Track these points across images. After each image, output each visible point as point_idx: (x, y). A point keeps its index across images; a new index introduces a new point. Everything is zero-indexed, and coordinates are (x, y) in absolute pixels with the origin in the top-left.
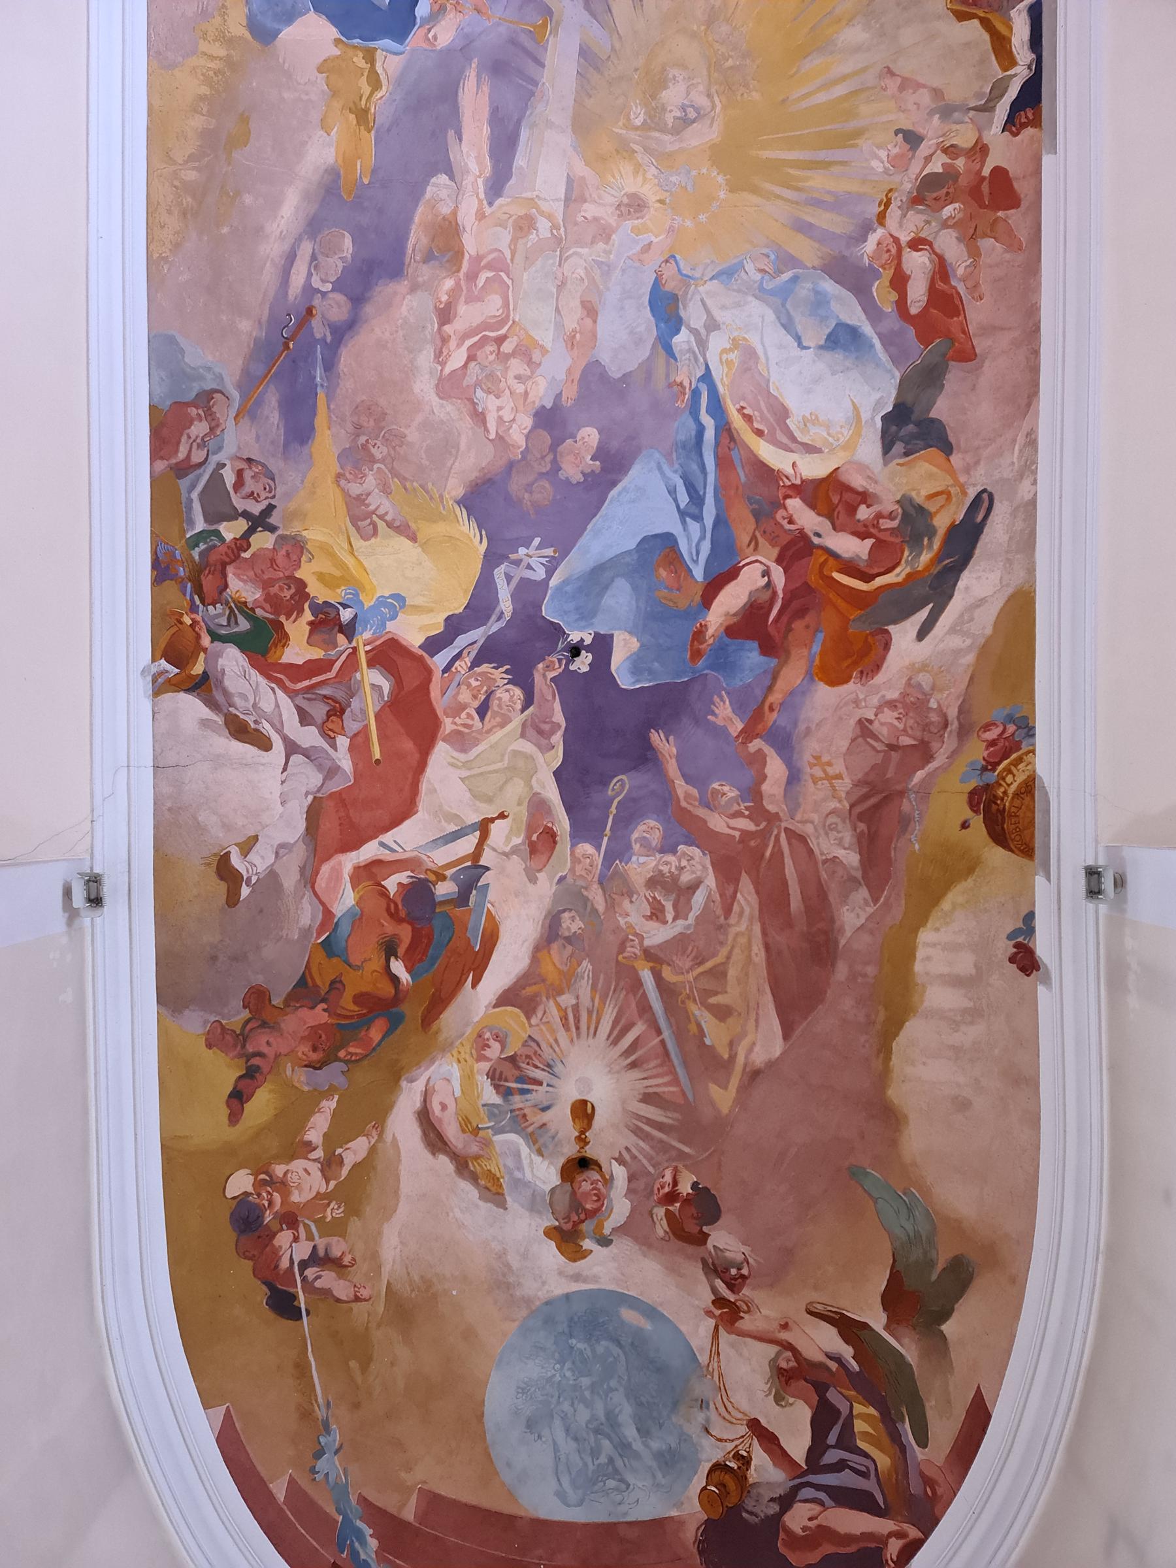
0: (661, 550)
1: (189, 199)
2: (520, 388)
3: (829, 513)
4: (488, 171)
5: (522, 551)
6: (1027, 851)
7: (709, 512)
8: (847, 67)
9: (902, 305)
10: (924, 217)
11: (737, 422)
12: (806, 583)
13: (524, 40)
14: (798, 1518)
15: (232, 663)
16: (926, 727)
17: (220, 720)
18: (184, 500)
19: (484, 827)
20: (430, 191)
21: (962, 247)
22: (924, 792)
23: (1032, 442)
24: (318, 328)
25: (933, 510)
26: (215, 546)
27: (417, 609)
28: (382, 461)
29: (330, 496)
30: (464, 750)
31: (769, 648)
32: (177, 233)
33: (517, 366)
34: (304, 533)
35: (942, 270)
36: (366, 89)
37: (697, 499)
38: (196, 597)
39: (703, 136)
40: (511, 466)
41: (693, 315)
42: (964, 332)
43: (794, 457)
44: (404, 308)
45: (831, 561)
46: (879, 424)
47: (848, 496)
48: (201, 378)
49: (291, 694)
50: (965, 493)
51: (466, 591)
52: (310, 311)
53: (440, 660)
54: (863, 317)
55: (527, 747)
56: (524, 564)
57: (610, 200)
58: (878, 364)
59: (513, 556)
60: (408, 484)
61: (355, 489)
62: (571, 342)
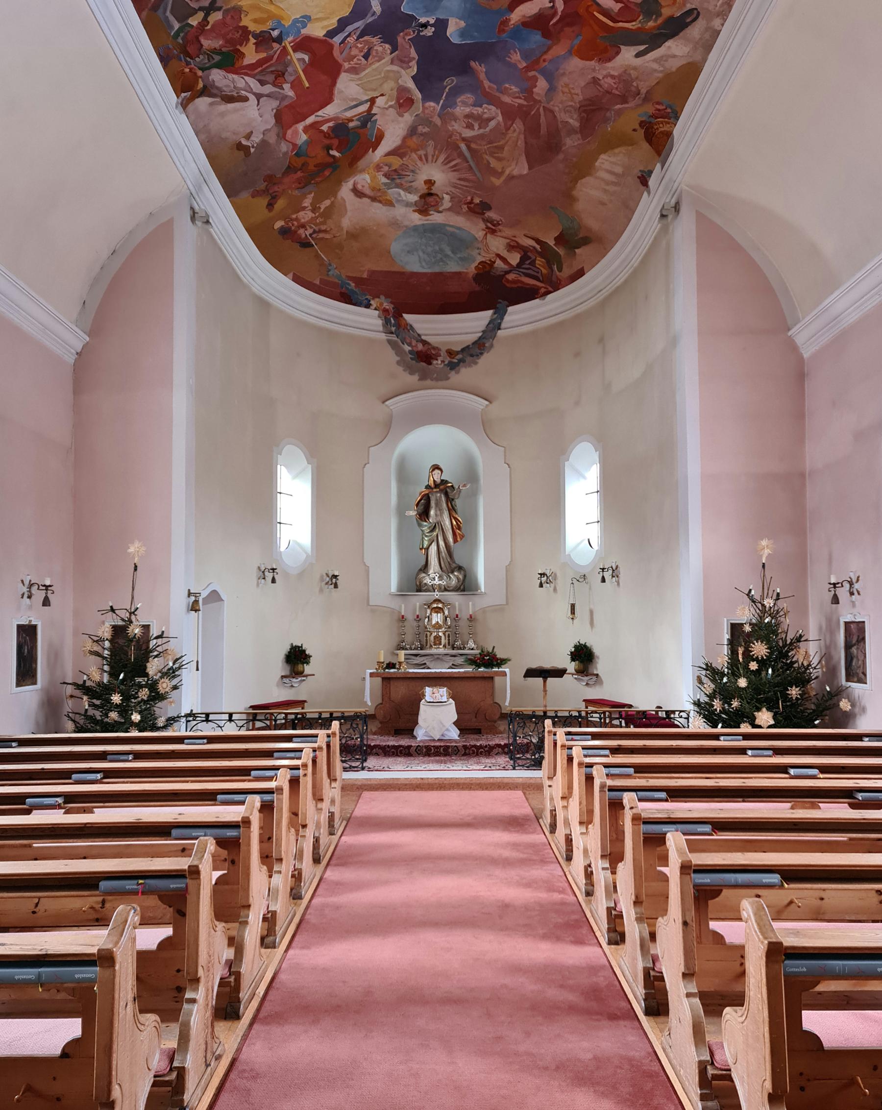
6: (659, 153)
14: (511, 277)
15: (217, 76)
19: (372, 101)
22: (619, 113)
30: (357, 74)
45: (595, 6)
50: (684, 5)
53: (337, 39)
55: (395, 68)
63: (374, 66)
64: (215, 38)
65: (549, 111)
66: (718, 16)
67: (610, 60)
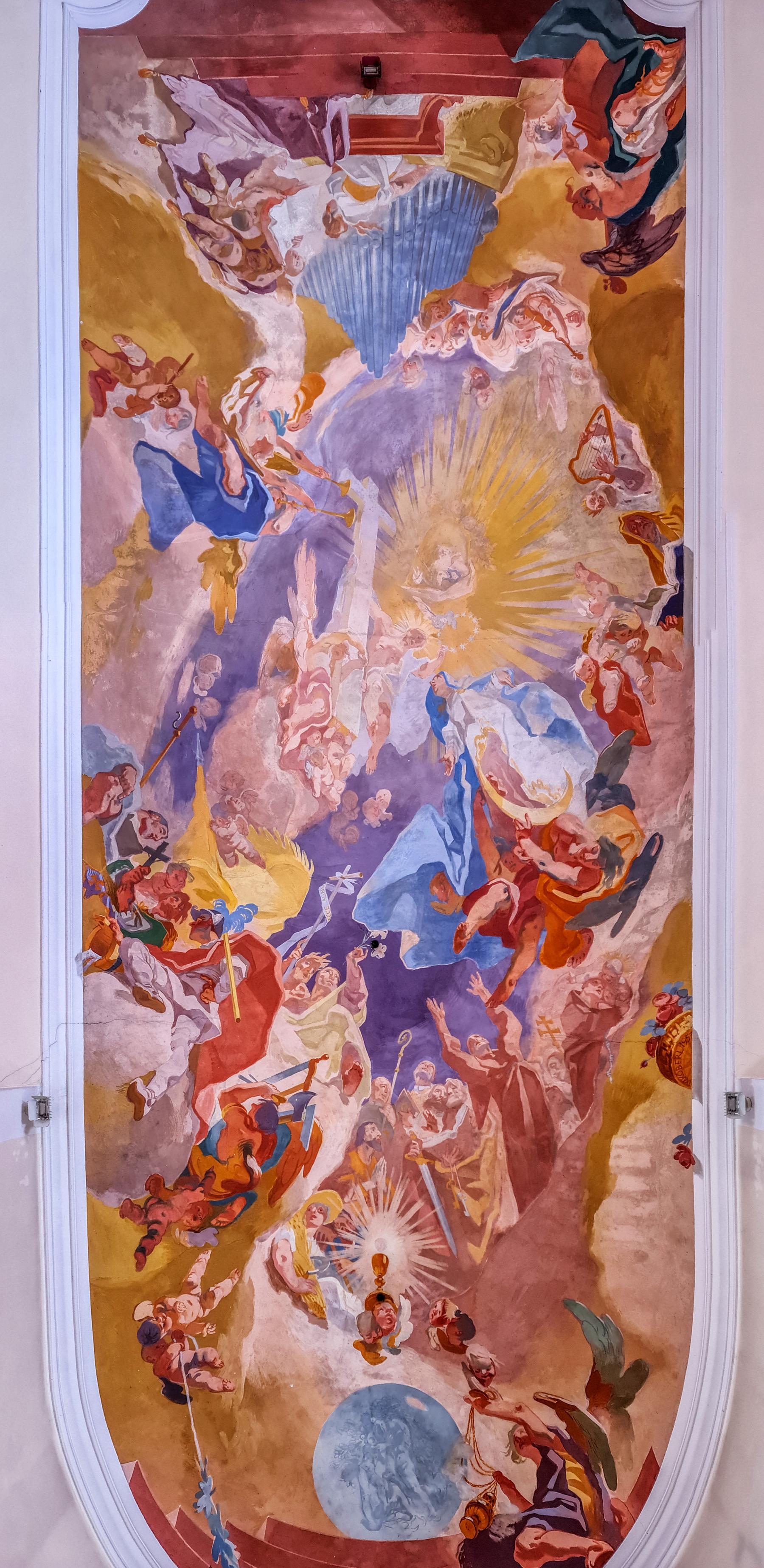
2: (337, 763)
3: (551, 850)
4: (315, 614)
5: (338, 874)
6: (687, 1082)
8: (553, 558)
12: (534, 897)
13: (338, 524)
15: (137, 952)
16: (617, 997)
18: (105, 839)
19: (311, 1065)
20: (275, 628)
22: (616, 1042)
24: (198, 722)
25: (621, 847)
26: (126, 871)
27: (266, 914)
28: (242, 812)
29: (206, 837)
31: (509, 941)
32: (102, 657)
33: (334, 747)
37: (459, 839)
40: (330, 815)
41: (456, 712)
44: (258, 707)
45: (552, 882)
48: (118, 756)
50: (643, 836)
51: (299, 902)
52: (192, 710)
53: (280, 950)
55: (342, 1010)
56: (339, 883)
59: (331, 878)
61: (223, 832)
62: (372, 731)
65: (529, 1073)
67: (584, 955)
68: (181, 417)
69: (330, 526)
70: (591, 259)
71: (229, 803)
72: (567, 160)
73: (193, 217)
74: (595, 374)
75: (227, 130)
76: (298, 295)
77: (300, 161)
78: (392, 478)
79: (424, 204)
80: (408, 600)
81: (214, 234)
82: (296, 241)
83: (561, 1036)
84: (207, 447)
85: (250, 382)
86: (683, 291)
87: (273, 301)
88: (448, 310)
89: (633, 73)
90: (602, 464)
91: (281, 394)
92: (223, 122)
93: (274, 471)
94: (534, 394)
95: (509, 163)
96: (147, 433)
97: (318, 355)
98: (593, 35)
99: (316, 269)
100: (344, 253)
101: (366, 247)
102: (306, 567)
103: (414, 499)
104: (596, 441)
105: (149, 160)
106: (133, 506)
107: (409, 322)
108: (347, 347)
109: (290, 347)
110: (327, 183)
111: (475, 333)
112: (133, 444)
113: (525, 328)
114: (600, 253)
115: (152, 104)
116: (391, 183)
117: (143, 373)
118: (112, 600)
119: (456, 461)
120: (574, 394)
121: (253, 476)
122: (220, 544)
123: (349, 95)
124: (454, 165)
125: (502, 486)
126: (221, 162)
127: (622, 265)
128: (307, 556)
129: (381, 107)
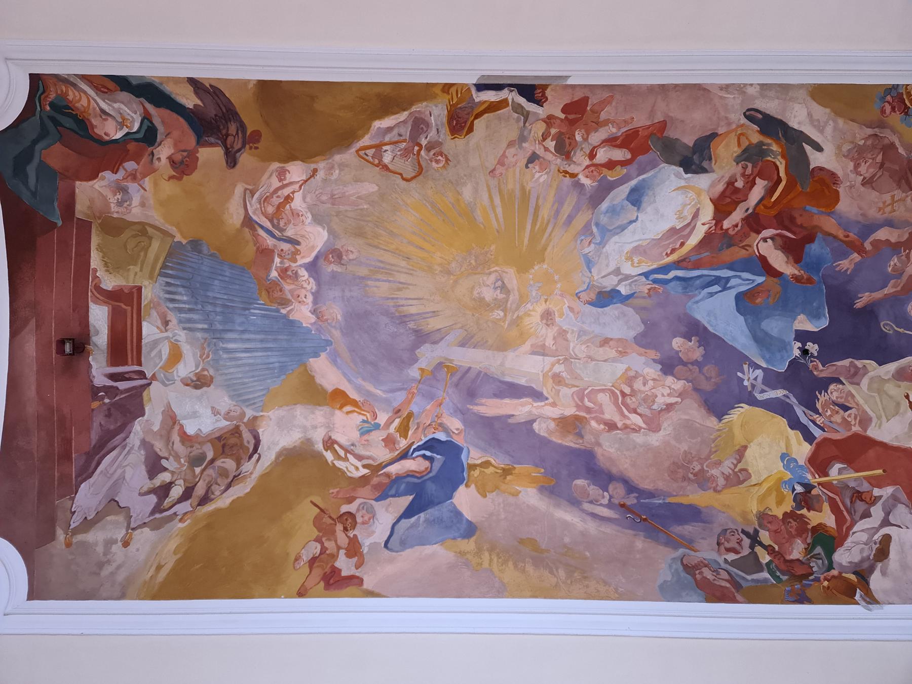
0: (745, 302)
1: (576, 574)
2: (651, 383)
3: (735, 204)
4: (529, 400)
5: (746, 383)
7: (725, 273)
8: (485, 196)
9: (623, 163)
10: (578, 151)
11: (674, 257)
12: (775, 217)
13: (455, 379)
15: (844, 557)
16: (874, 147)
17: (879, 565)
18: (753, 584)
20: (543, 433)
21: (600, 130)
23: (726, 88)
24: (631, 501)
25: (747, 143)
26: (776, 566)
27: (788, 445)
28: (702, 465)
29: (729, 497)
30: (870, 420)
31: (810, 239)
32: (598, 582)
33: (638, 385)
34: (754, 512)
35: (611, 142)
36: (491, 470)
37: (717, 280)
38: (811, 578)
39: (511, 277)
40: (696, 389)
41: (610, 283)
42: (649, 127)
43: (699, 224)
44: (609, 449)
45: (764, 202)
46: (689, 175)
47: (728, 193)
48: (676, 570)
49: (853, 523)
50: (742, 125)
51: (773, 417)
52: (623, 506)
53: (817, 433)
54: (626, 185)
55: (865, 382)
56: (754, 382)
57: (544, 331)
58: (655, 176)
59: (750, 389)
60: (713, 450)
61: (721, 481)
62: (623, 353)
63: (861, 402)
64: (791, 545)
66: (745, 92)
68: (364, 511)
69: (457, 385)
70: (232, 160)
71: (695, 475)
72: (147, 179)
73: (194, 500)
74: (329, 158)
75: (119, 471)
76: (262, 411)
77: (147, 409)
78: (417, 332)
79: (184, 303)
80: (516, 322)
81: (209, 482)
82: (215, 412)
83: (899, 194)
84: (390, 490)
85: (335, 452)
86: (259, 81)
87: (266, 434)
88: (275, 284)
89: (71, 120)
90: (406, 153)
91: (345, 426)
92: (113, 474)
93: (410, 433)
94: (346, 211)
95: (150, 230)
96: (377, 541)
97: (314, 394)
98: (37, 155)
99: (240, 395)
100: (226, 372)
101: (221, 353)
102: (491, 407)
103: (435, 313)
104: (387, 159)
105: (144, 538)
106: (438, 553)
107: (285, 317)
108: (306, 370)
109: (306, 418)
110: (166, 385)
111: (295, 261)
112: (386, 552)
113: (291, 218)
114: (227, 153)
115: (95, 536)
116: (166, 331)
117: (327, 544)
118: (546, 573)
119: (403, 278)
120: (345, 176)
121: (415, 450)
122: (472, 479)
123: (90, 366)
124: (151, 277)
125: (424, 239)
126: (147, 476)
127: (237, 133)
128: (482, 405)
129: (101, 336)
